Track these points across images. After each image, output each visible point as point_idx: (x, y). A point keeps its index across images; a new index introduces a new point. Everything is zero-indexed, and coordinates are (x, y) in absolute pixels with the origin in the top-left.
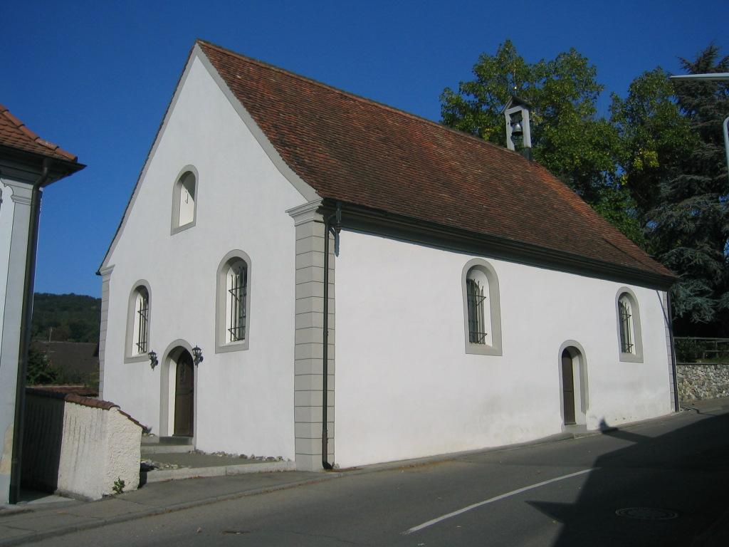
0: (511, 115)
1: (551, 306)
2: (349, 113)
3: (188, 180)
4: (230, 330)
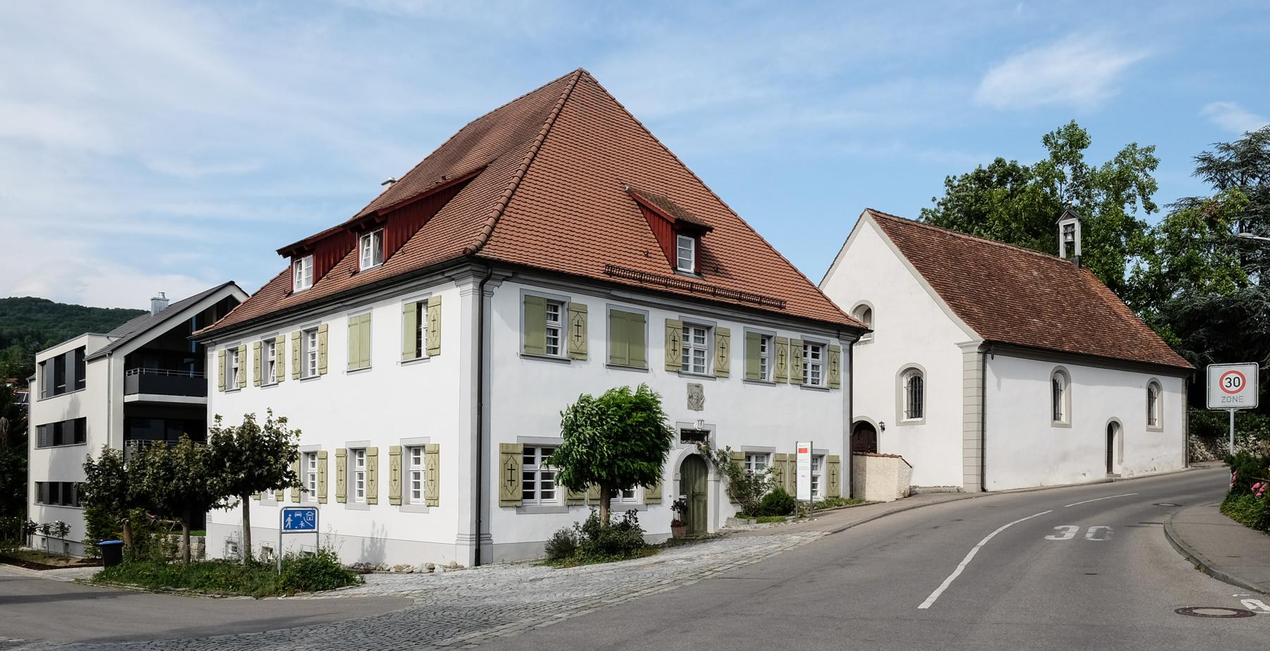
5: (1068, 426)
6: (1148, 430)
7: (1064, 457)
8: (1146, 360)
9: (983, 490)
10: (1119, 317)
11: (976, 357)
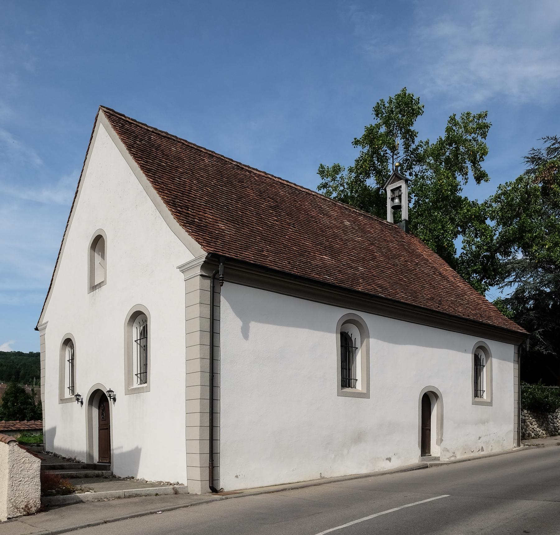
0: (391, 190)
1: (407, 361)
2: (243, 182)
3: (98, 243)
4: (484, 391)
5: (365, 395)
6: (474, 403)
7: (358, 437)
8: (471, 317)
9: (214, 490)
10: (444, 278)
11: (199, 284)
